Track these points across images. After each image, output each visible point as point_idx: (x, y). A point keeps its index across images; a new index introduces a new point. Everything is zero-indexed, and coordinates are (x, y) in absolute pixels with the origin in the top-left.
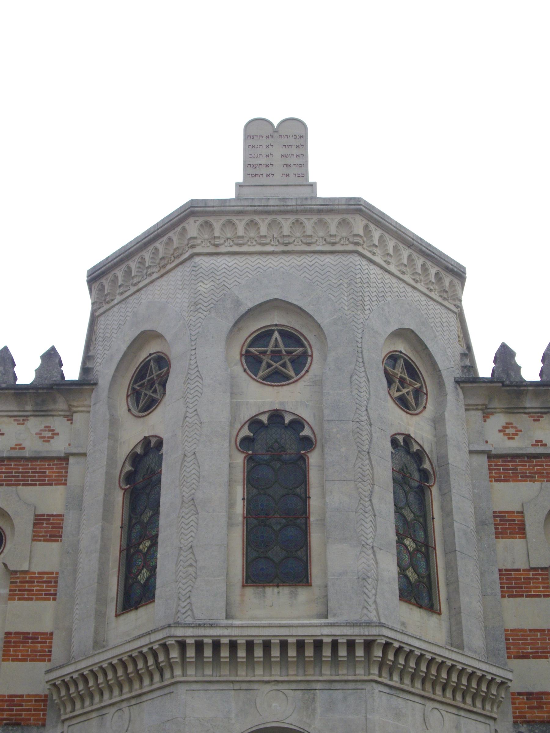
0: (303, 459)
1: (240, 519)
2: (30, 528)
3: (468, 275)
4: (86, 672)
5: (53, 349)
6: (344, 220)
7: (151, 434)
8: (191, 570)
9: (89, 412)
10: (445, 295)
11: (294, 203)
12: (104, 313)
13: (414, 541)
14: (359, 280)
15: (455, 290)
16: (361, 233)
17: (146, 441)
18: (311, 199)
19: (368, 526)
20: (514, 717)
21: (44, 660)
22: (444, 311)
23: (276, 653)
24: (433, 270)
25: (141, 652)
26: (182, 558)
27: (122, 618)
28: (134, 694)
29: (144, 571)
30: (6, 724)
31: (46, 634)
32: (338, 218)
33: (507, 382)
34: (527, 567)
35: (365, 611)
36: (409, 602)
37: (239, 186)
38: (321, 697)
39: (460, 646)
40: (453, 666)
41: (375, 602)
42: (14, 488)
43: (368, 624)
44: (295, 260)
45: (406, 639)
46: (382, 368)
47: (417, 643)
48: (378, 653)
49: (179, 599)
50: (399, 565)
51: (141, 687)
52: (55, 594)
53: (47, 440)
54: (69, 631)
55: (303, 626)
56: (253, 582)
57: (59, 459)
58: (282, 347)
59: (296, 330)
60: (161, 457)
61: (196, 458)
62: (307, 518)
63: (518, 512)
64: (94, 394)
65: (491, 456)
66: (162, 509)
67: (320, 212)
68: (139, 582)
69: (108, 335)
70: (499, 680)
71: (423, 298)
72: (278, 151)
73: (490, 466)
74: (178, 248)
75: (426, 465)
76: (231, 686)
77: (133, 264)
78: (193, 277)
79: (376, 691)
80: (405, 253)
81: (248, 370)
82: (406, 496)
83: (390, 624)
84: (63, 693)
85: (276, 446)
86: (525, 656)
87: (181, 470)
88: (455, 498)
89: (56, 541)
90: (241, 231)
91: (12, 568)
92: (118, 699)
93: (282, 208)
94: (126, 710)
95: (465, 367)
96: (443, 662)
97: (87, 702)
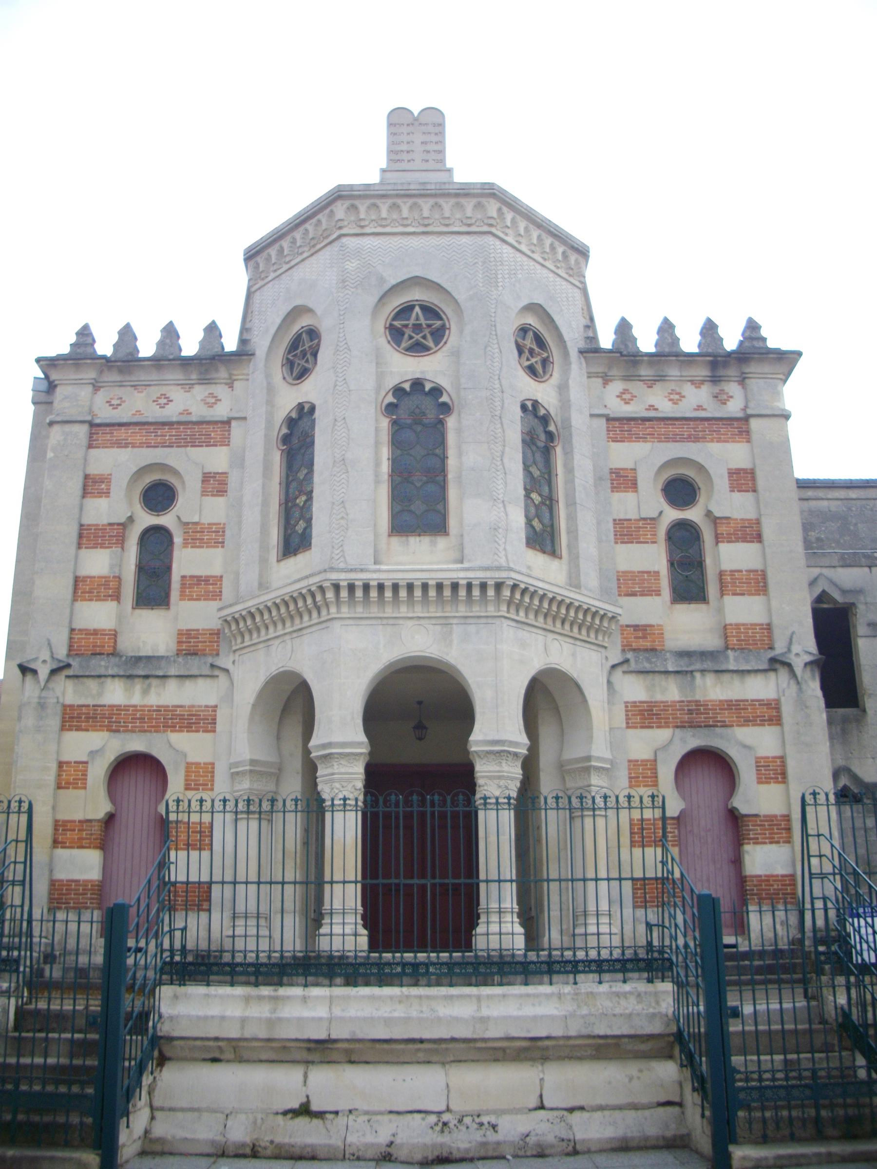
0: (441, 422)
1: (386, 477)
2: (199, 485)
3: (592, 254)
4: (253, 610)
5: (213, 322)
6: (479, 203)
7: (304, 400)
8: (343, 522)
9: (248, 380)
10: (571, 272)
11: (433, 187)
12: (259, 289)
13: (540, 495)
14: (493, 259)
15: (580, 268)
16: (495, 215)
17: (300, 407)
18: (449, 183)
19: (499, 482)
20: (622, 646)
21: (216, 600)
22: (570, 286)
23: (418, 593)
24: (560, 249)
25: (301, 593)
26: (334, 511)
27: (283, 563)
28: (295, 628)
29: (301, 522)
30: (186, 654)
31: (216, 577)
32: (474, 201)
33: (625, 353)
34: (637, 517)
35: (496, 557)
36: (534, 548)
37: (383, 171)
38: (457, 630)
39: (578, 586)
40: (571, 603)
41: (505, 549)
42: (183, 449)
43: (499, 568)
44: (433, 240)
45: (531, 581)
46: (513, 340)
47: (540, 584)
48: (507, 593)
49: (333, 547)
50: (526, 516)
51: (301, 623)
52: (223, 543)
53: (211, 406)
54: (237, 574)
55: (441, 570)
56: (397, 532)
57: (223, 422)
58: (423, 321)
59: (436, 305)
60: (314, 421)
61: (345, 423)
62: (445, 476)
63: (631, 469)
64: (252, 364)
65: (609, 419)
66: (316, 467)
67: (457, 195)
68: (297, 532)
69: (263, 309)
70: (610, 615)
71: (551, 275)
72: (418, 138)
73: (608, 427)
74: (326, 230)
75: (552, 428)
76: (379, 622)
77: (285, 243)
78: (341, 256)
79: (505, 625)
80: (535, 233)
81: (392, 342)
82: (534, 455)
83: (517, 568)
84: (234, 627)
85: (417, 411)
86: (634, 594)
87: (332, 432)
88: (577, 457)
89: (223, 496)
90: (384, 214)
91: (184, 520)
92: (282, 632)
93: (422, 192)
94: (289, 642)
95: (588, 338)
96: (563, 600)
97: (255, 635)
